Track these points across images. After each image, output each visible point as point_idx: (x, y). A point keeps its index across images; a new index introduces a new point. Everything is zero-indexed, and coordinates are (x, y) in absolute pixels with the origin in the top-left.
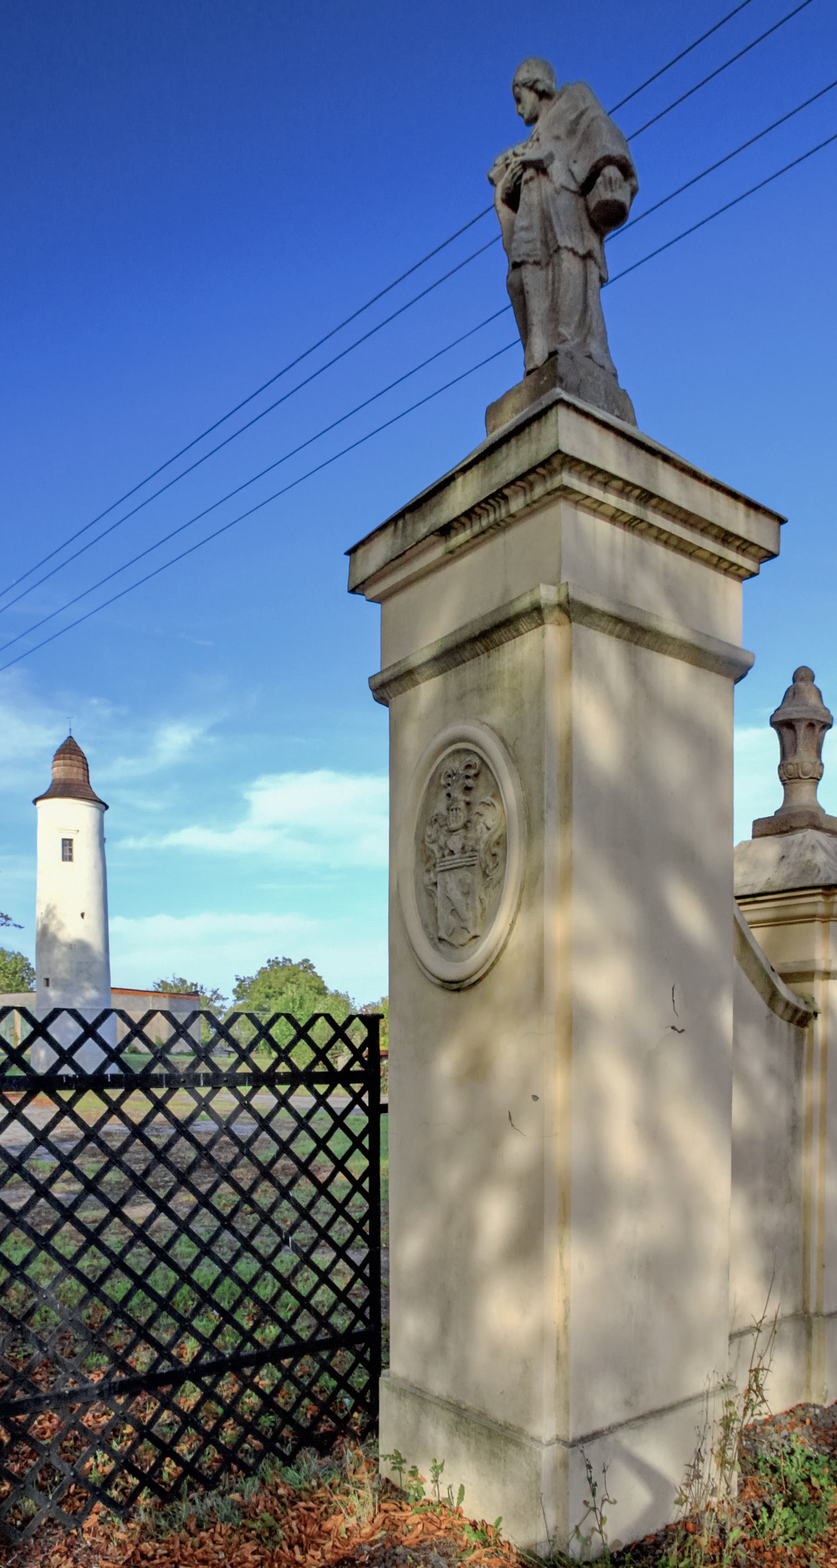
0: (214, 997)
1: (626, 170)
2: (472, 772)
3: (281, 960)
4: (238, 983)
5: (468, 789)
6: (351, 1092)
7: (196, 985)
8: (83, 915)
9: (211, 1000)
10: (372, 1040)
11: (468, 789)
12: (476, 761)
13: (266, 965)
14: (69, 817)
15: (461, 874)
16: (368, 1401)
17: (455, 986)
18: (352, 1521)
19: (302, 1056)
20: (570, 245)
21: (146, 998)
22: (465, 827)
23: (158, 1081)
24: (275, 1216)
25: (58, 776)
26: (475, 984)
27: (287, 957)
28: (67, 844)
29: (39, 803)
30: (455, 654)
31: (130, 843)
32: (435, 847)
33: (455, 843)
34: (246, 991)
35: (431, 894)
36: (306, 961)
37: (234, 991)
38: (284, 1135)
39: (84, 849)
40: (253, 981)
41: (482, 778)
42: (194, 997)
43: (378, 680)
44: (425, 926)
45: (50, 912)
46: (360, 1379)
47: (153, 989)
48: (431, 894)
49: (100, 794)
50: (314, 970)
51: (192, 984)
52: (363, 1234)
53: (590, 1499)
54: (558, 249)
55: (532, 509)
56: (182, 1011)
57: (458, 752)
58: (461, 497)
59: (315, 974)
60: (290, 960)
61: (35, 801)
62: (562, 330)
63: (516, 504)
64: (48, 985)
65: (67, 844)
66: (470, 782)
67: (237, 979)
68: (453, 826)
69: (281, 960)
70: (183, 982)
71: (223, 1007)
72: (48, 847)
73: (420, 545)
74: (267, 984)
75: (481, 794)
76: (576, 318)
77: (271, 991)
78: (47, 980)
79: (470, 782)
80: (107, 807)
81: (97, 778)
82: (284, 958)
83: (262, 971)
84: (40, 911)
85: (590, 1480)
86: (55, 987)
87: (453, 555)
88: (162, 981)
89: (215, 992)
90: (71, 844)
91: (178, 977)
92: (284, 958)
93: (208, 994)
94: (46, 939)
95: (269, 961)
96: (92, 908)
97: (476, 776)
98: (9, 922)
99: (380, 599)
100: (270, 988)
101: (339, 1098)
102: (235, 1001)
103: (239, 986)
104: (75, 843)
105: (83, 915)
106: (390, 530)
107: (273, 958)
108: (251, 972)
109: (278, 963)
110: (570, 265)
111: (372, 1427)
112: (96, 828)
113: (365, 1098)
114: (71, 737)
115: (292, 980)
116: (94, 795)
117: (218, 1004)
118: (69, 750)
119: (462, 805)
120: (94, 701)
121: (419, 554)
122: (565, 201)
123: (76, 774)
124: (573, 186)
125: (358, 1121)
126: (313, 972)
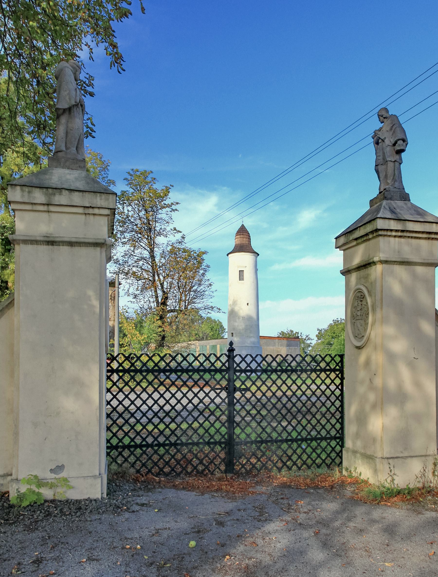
0: (307, 338)
1: (404, 141)
2: (362, 297)
4: (318, 331)
5: (361, 301)
6: (336, 374)
7: (298, 333)
8: (248, 304)
9: (305, 339)
10: (342, 361)
11: (361, 301)
12: (363, 294)
13: (332, 322)
14: (243, 260)
15: (360, 321)
16: (340, 455)
17: (359, 348)
18: (333, 479)
19: (323, 365)
20: (390, 160)
21: (275, 341)
22: (361, 310)
23: (280, 371)
24: (316, 404)
26: (362, 347)
28: (241, 273)
29: (229, 255)
30: (360, 268)
31: (276, 267)
32: (355, 314)
33: (359, 313)
34: (322, 336)
35: (354, 325)
37: (317, 336)
38: (333, 401)
39: (248, 275)
40: (326, 331)
41: (364, 299)
43: (342, 271)
44: (353, 333)
45: (235, 303)
46: (338, 448)
47: (276, 336)
48: (354, 325)
49: (256, 250)
51: (296, 333)
52: (339, 411)
53: (390, 473)
54: (387, 161)
55: (374, 238)
56: (292, 346)
57: (359, 292)
58: (357, 234)
61: (228, 255)
62: (388, 181)
63: (371, 236)
64: (233, 336)
65: (241, 273)
66: (362, 299)
68: (358, 309)
70: (292, 331)
71: (311, 343)
72: (233, 274)
73: (351, 241)
74: (333, 331)
75: (364, 303)
76: (392, 178)
77: (334, 335)
78: (233, 333)
79: (362, 299)
80: (258, 255)
81: (254, 244)
83: (331, 325)
84: (231, 302)
85: (390, 468)
86: (236, 336)
87: (358, 244)
88: (282, 332)
89: (307, 336)
90: (243, 273)
91: (289, 329)
93: (304, 337)
94: (232, 314)
95: (333, 321)
96: (252, 302)
97: (363, 298)
98: (220, 311)
99: (344, 250)
100: (334, 334)
101: (333, 375)
102: (317, 340)
103: (319, 333)
104: (245, 273)
105: (248, 304)
106: (344, 236)
108: (325, 326)
109: (338, 321)
110: (391, 165)
111: (341, 463)
112: (254, 264)
113: (340, 376)
117: (308, 342)
118: (243, 231)
119: (360, 305)
121: (350, 243)
122: (388, 149)
123: (245, 241)
124: (391, 145)
125: (338, 381)
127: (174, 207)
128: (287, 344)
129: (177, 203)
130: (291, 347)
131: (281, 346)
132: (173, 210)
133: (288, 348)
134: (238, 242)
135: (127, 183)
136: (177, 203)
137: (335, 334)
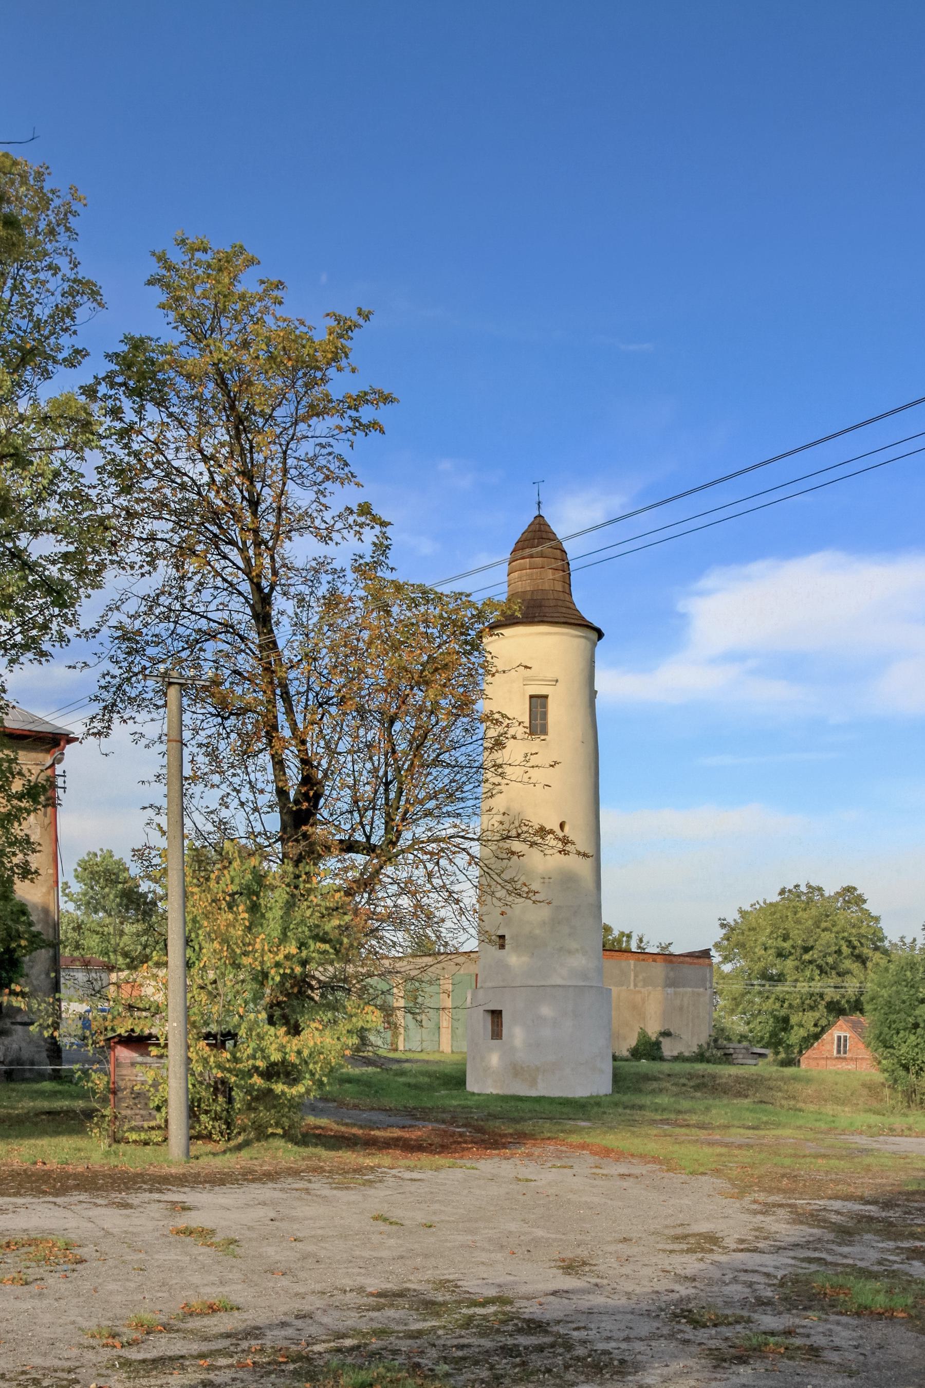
3: (803, 889)
4: (724, 931)
21: (624, 964)
25: (519, 587)
27: (813, 884)
36: (850, 890)
42: (701, 960)
50: (865, 906)
51: (622, 934)
59: (867, 913)
60: (820, 889)
64: (502, 947)
67: (723, 926)
69: (803, 889)
80: (600, 635)
81: (584, 601)
82: (809, 886)
90: (545, 706)
92: (809, 886)
95: (782, 892)
98: (569, 847)
100: (784, 940)
107: (790, 886)
114: (540, 516)
115: (824, 925)
116: (583, 618)
120: (446, 465)
123: (548, 579)
126: (862, 909)
127: (367, 413)
128: (667, 977)
129: (387, 399)
130: (681, 990)
131: (646, 983)
132: (367, 428)
133: (670, 990)
134: (524, 586)
135: (163, 298)
136: (387, 399)
137: (790, 942)
